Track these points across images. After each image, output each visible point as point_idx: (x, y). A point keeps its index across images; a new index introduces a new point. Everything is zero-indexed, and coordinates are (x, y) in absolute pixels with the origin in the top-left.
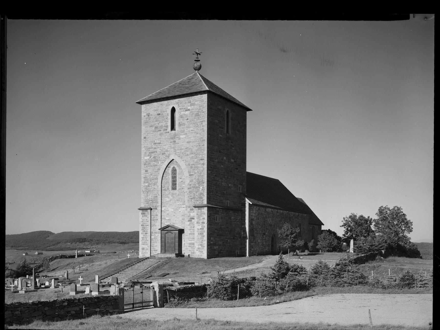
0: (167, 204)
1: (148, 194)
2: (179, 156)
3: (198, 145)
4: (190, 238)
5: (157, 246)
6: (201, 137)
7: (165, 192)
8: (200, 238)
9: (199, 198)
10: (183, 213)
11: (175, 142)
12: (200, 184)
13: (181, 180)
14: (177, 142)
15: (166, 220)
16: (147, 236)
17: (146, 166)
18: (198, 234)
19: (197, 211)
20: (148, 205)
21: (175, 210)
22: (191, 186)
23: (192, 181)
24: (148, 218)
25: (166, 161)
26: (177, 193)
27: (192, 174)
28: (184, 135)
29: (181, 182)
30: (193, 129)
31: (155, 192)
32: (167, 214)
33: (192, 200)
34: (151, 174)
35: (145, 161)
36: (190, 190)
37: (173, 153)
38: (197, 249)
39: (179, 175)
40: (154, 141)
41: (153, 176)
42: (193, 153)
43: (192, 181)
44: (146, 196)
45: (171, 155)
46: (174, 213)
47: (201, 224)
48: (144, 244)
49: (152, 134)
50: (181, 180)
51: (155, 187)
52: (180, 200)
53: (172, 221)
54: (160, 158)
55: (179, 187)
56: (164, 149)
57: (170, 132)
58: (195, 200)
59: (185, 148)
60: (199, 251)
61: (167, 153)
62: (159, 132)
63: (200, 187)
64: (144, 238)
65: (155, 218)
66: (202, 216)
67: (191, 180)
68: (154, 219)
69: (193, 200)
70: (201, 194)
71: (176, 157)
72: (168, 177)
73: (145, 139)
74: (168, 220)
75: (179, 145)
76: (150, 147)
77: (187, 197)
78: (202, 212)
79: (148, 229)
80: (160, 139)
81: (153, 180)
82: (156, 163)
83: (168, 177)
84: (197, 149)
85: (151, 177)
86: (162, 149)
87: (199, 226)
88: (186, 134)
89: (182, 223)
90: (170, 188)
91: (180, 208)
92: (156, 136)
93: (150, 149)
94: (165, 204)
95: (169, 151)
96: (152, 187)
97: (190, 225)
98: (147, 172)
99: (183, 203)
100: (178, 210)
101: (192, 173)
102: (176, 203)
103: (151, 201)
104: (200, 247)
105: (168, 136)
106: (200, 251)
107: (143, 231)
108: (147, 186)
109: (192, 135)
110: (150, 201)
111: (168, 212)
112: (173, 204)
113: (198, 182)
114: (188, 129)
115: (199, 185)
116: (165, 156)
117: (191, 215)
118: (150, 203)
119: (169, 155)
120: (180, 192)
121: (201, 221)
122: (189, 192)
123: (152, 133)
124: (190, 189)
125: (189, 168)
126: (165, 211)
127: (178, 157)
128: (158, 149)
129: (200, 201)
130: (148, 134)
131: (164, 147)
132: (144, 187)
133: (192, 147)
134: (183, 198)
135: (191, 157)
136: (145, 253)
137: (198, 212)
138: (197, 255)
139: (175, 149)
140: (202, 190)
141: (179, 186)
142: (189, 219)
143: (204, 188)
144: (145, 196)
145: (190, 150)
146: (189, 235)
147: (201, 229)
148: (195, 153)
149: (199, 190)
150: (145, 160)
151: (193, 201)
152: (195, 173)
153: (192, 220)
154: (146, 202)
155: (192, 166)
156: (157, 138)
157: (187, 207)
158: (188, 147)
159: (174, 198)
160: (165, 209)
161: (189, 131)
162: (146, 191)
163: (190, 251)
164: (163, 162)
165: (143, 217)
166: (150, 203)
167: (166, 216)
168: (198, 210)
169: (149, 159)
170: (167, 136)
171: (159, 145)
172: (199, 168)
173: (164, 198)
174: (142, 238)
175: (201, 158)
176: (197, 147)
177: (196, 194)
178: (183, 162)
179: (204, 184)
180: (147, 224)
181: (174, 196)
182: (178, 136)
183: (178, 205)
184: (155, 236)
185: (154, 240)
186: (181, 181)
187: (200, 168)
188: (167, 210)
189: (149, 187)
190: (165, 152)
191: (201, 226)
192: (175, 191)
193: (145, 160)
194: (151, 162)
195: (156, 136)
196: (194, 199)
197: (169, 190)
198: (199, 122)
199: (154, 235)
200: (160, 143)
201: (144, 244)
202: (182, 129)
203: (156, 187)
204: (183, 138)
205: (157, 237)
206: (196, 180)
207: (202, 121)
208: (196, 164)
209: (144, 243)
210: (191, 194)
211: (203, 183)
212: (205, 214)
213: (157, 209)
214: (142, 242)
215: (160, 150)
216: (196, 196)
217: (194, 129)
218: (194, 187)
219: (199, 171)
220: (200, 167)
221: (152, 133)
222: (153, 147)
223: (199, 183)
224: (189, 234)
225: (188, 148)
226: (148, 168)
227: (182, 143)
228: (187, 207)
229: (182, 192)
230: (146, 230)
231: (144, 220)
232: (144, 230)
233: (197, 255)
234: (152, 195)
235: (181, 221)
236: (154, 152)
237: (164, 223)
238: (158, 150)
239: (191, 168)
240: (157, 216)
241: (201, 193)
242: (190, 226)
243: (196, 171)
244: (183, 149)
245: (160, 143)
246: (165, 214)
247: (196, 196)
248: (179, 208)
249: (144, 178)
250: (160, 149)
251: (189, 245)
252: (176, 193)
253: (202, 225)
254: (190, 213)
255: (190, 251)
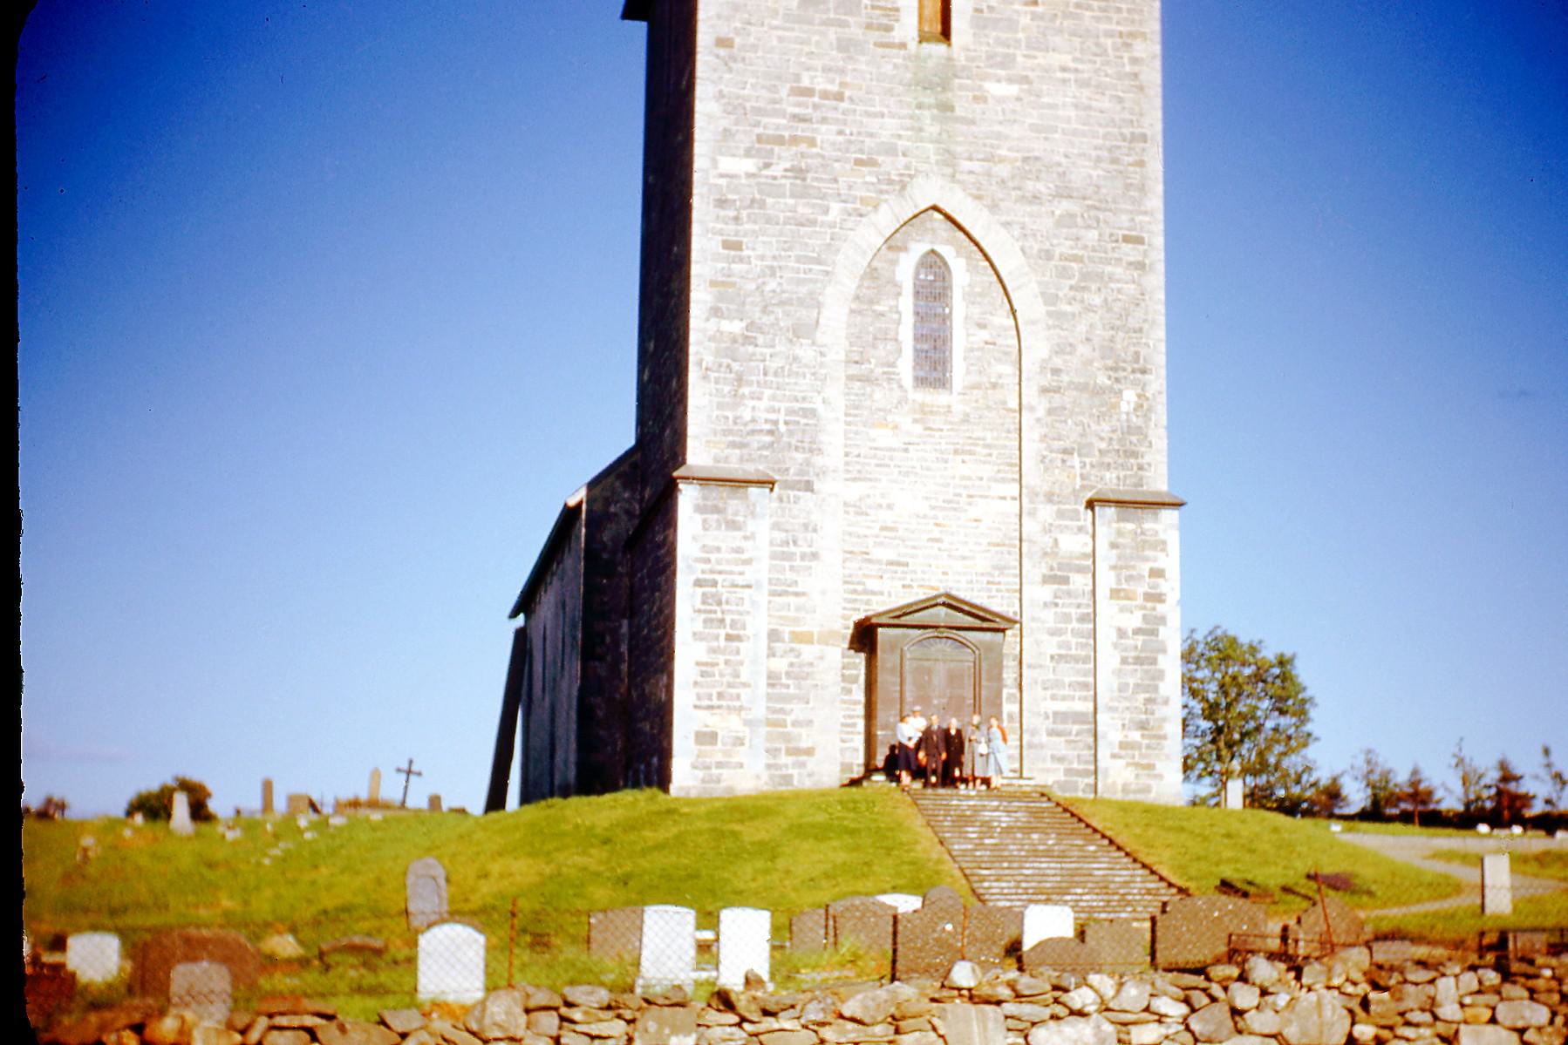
0: (878, 465)
1: (745, 390)
2: (974, 192)
3: (1105, 154)
4: (1058, 684)
5: (810, 722)
6: (1127, 116)
7: (868, 389)
8: (1137, 686)
9: (1118, 451)
10: (999, 529)
11: (946, 107)
12: (1125, 378)
13: (984, 335)
14: (959, 112)
15: (879, 562)
16: (738, 653)
17: (731, 213)
18: (1119, 660)
19: (1115, 525)
20: (741, 460)
21: (944, 509)
22: (1065, 378)
23: (1068, 349)
24: (746, 538)
25: (884, 208)
26: (958, 408)
27: (1068, 308)
28: (1010, 80)
29: (982, 345)
30: (1072, 65)
31: (801, 381)
32: (883, 529)
33: (1065, 457)
34: (772, 268)
35: (723, 181)
36: (1057, 400)
37: (935, 168)
38: (1116, 750)
39: (973, 303)
40: (797, 78)
41: (780, 284)
42: (1075, 194)
43: (1070, 353)
44: (727, 400)
45: (920, 180)
46: (936, 525)
47: (1140, 601)
48: (711, 707)
49: (780, 33)
50: (984, 335)
51: (799, 352)
52: (979, 449)
53: (920, 575)
54: (836, 181)
55: (968, 372)
56: (871, 135)
57: (913, 45)
58: (1088, 460)
59: (1019, 155)
60: (1128, 765)
61: (891, 166)
62: (832, 34)
63: (1121, 391)
64: (716, 670)
65: (800, 543)
66: (1146, 559)
67: (1058, 345)
68: (792, 548)
69: (1076, 460)
70: (1133, 435)
71: (959, 194)
72: (893, 303)
73: (722, 52)
74: (891, 563)
75: (974, 128)
76: (761, 104)
77: (1036, 436)
78: (1143, 533)
79: (748, 613)
80: (842, 71)
81: (781, 303)
82: (808, 211)
83: (893, 303)
84: (1098, 176)
85: (772, 285)
86: (855, 131)
87: (1127, 615)
88: (1025, 80)
89: (994, 587)
90: (906, 367)
91: (976, 499)
92: (806, 49)
93: (765, 120)
94: (869, 464)
95: (904, 155)
96: (773, 346)
97: (1056, 605)
98: (741, 250)
99: (999, 471)
100: (966, 511)
101: (1070, 304)
102: (946, 469)
103: (771, 432)
104: (1136, 736)
105: (896, 66)
106: (1137, 765)
107: (705, 621)
108: (740, 340)
109: (1065, 96)
110: (761, 431)
111: (886, 517)
112: (928, 469)
113: (1110, 363)
114: (1035, 57)
115: (1117, 380)
116: (875, 180)
117: (1061, 545)
118: (756, 445)
119: (902, 175)
120: (977, 401)
121: (1141, 589)
122: (1050, 412)
123: (776, 28)
124: (1055, 392)
125: (1044, 275)
126: (870, 507)
127: (970, 199)
128: (824, 128)
129: (1122, 474)
130: (752, 29)
131: (873, 124)
132: (709, 340)
133: (1063, 160)
134: (1001, 442)
135: (1058, 212)
136: (720, 765)
137: (1120, 533)
138: (1114, 783)
139: (948, 151)
140: (1135, 410)
141: (972, 368)
142: (1052, 569)
143: (1147, 399)
144: (716, 400)
145: (1055, 176)
146: (1052, 665)
147: (1137, 632)
148: (1084, 198)
149: (1116, 406)
150: (722, 176)
151: (1073, 467)
152: (1090, 309)
153: (1070, 575)
154: (730, 438)
155: (1067, 263)
156: (818, 63)
157: (1037, 495)
158: (1036, 154)
159: (930, 436)
160: (869, 496)
161: (1047, 71)
162: (728, 366)
163: (1061, 759)
164: (864, 209)
165: (705, 529)
166: (759, 449)
167: (871, 541)
168: (1119, 521)
169: (749, 175)
170: (890, 67)
171: (836, 109)
172: (1112, 285)
173: (861, 428)
174: (698, 664)
175: (1127, 233)
176: (1102, 165)
177: (1094, 427)
178: (1003, 231)
179: (1147, 376)
180: (740, 580)
181: (936, 421)
182: (968, 78)
183: (963, 478)
184: (798, 656)
185: (788, 687)
186: (987, 343)
187: (1119, 285)
188: (884, 502)
189: (751, 349)
190: (879, 154)
191: (1139, 614)
192: (938, 398)
193: (722, 176)
194: (769, 195)
195: (806, 49)
196: (1080, 455)
197: (901, 387)
198: (1109, 34)
199: (792, 650)
200: (839, 97)
201: (711, 707)
202: (1000, 50)
203: (805, 352)
204: (1001, 100)
205: (811, 664)
206: (1094, 350)
207: (1131, 35)
208: (1091, 259)
209: (715, 702)
210: (1061, 422)
211: (1144, 372)
212: (1169, 548)
213: (812, 491)
214: (702, 691)
215: (841, 138)
216: (1094, 440)
217: (1080, 67)
218: (1082, 388)
219: (1115, 300)
220: (1118, 281)
221: (776, 28)
222: (784, 106)
223: (1115, 369)
224: (1052, 657)
225: (1037, 159)
226: (748, 226)
227: (1001, 123)
228: (1037, 495)
229: (988, 408)
230: (728, 619)
231: (718, 549)
232: (719, 615)
233: (1114, 783)
234: (773, 398)
235: (985, 579)
236: (795, 140)
237: (859, 583)
238: (826, 133)
239: (1063, 273)
240: (815, 530)
241: (1129, 427)
242: (1058, 610)
243: (1097, 300)
244: (1002, 160)
245: (839, 97)
246: (869, 527)
247: (1094, 440)
248: (970, 496)
249: (713, 283)
250: (840, 133)
251: (1049, 724)
252: (949, 407)
253: (1144, 608)
254: (1053, 535)
255: (1061, 759)
